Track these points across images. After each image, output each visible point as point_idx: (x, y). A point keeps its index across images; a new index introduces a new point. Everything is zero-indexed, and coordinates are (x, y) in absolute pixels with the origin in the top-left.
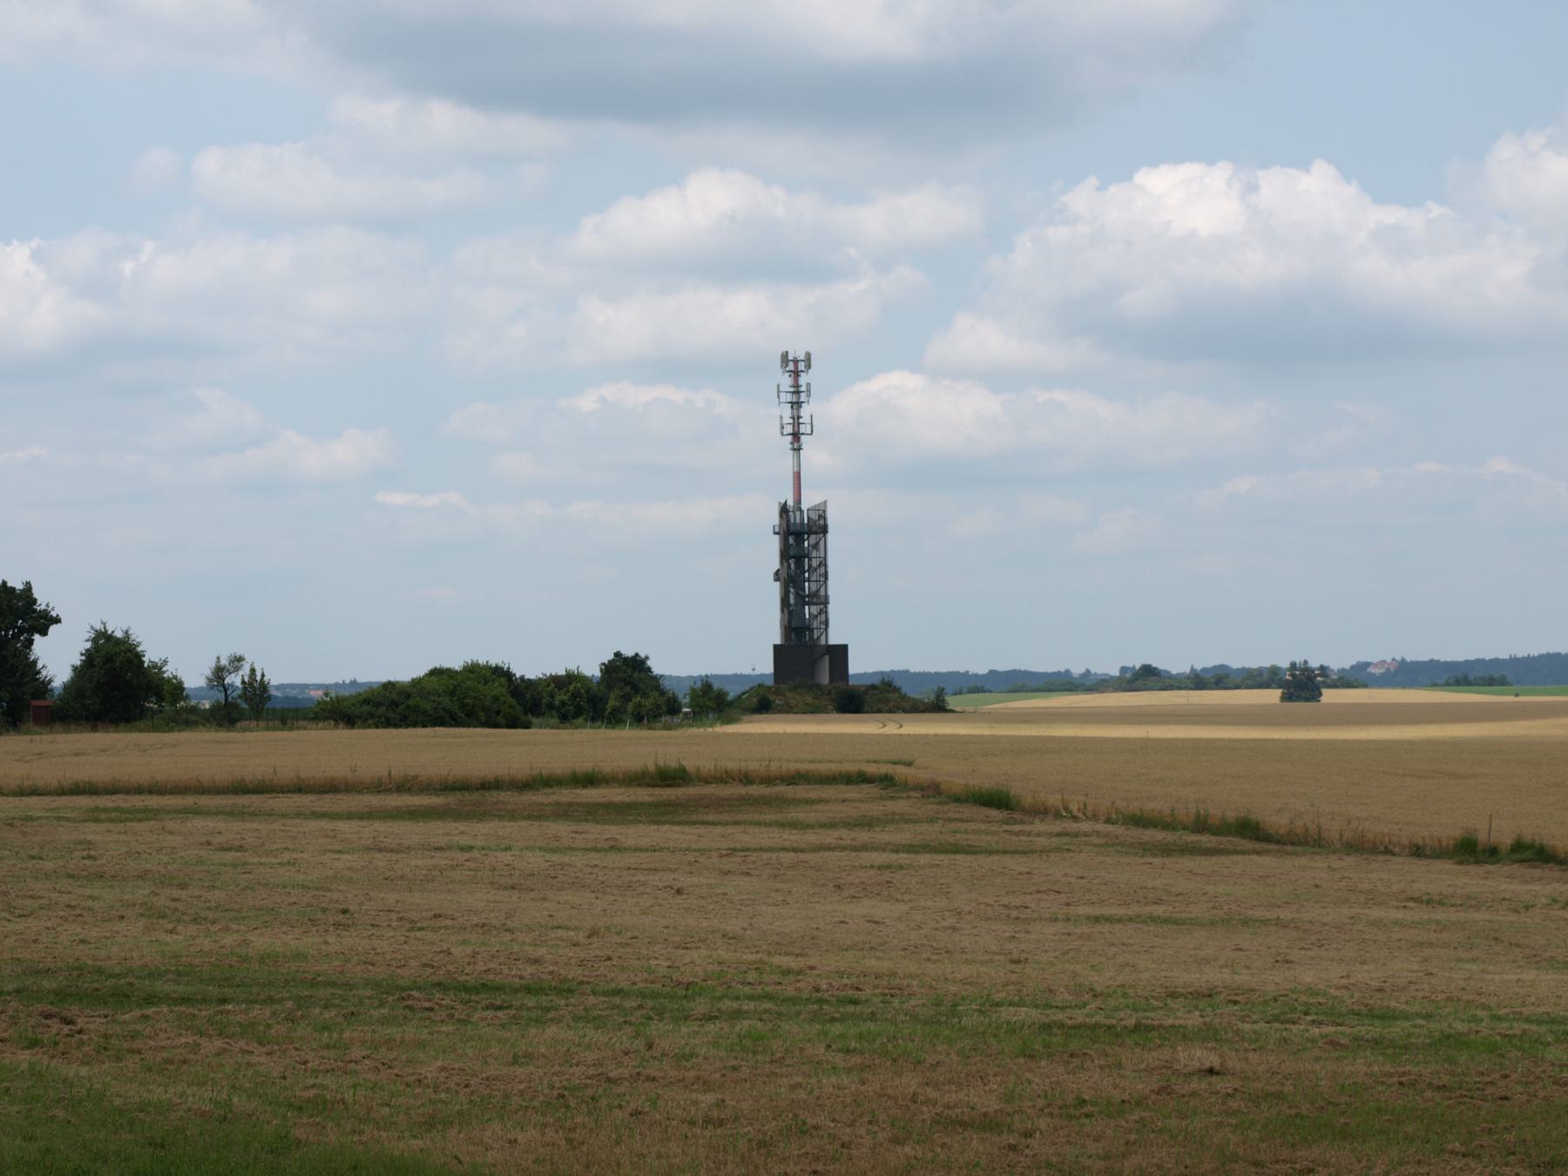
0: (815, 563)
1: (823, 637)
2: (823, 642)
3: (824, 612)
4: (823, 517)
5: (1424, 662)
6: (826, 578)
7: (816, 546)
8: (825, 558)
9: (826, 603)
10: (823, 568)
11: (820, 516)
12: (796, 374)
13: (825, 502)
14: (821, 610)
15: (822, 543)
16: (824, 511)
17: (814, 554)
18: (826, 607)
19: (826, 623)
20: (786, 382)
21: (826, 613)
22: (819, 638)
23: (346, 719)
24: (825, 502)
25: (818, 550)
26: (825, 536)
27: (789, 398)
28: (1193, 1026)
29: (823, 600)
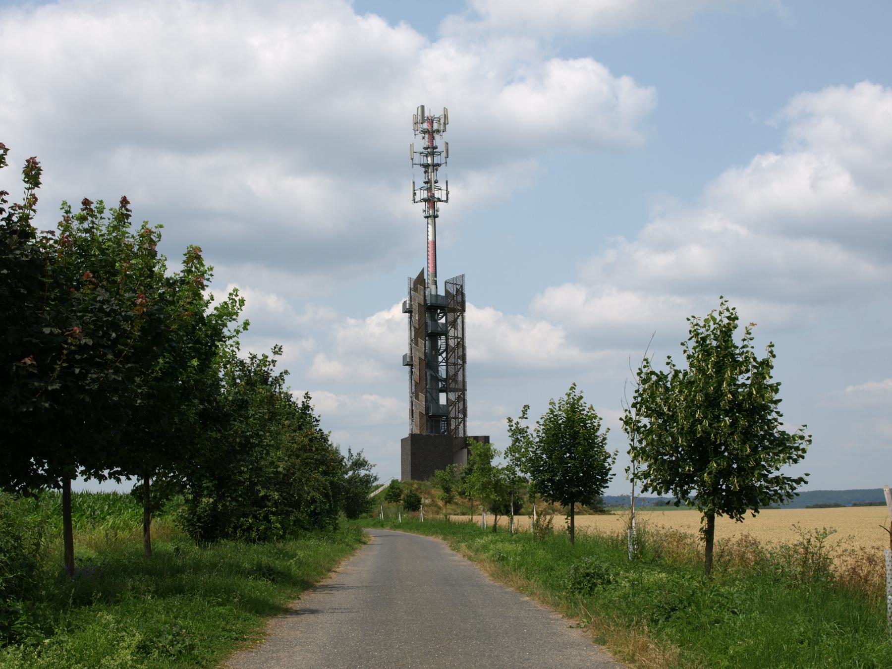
0: (452, 343)
1: (461, 427)
2: (461, 435)
3: (462, 399)
4: (460, 292)
5: (614, 497)
6: (465, 415)
7: (454, 324)
8: (463, 339)
9: (464, 390)
10: (461, 404)
11: (457, 290)
12: (431, 133)
13: (463, 276)
14: (459, 396)
15: (459, 321)
16: (462, 286)
17: (451, 333)
18: (464, 394)
19: (464, 411)
20: (421, 143)
21: (464, 401)
22: (457, 428)
23: (565, 572)
24: (463, 276)
25: (455, 328)
26: (462, 314)
27: (425, 194)
28: (301, 540)
29: (460, 386)
